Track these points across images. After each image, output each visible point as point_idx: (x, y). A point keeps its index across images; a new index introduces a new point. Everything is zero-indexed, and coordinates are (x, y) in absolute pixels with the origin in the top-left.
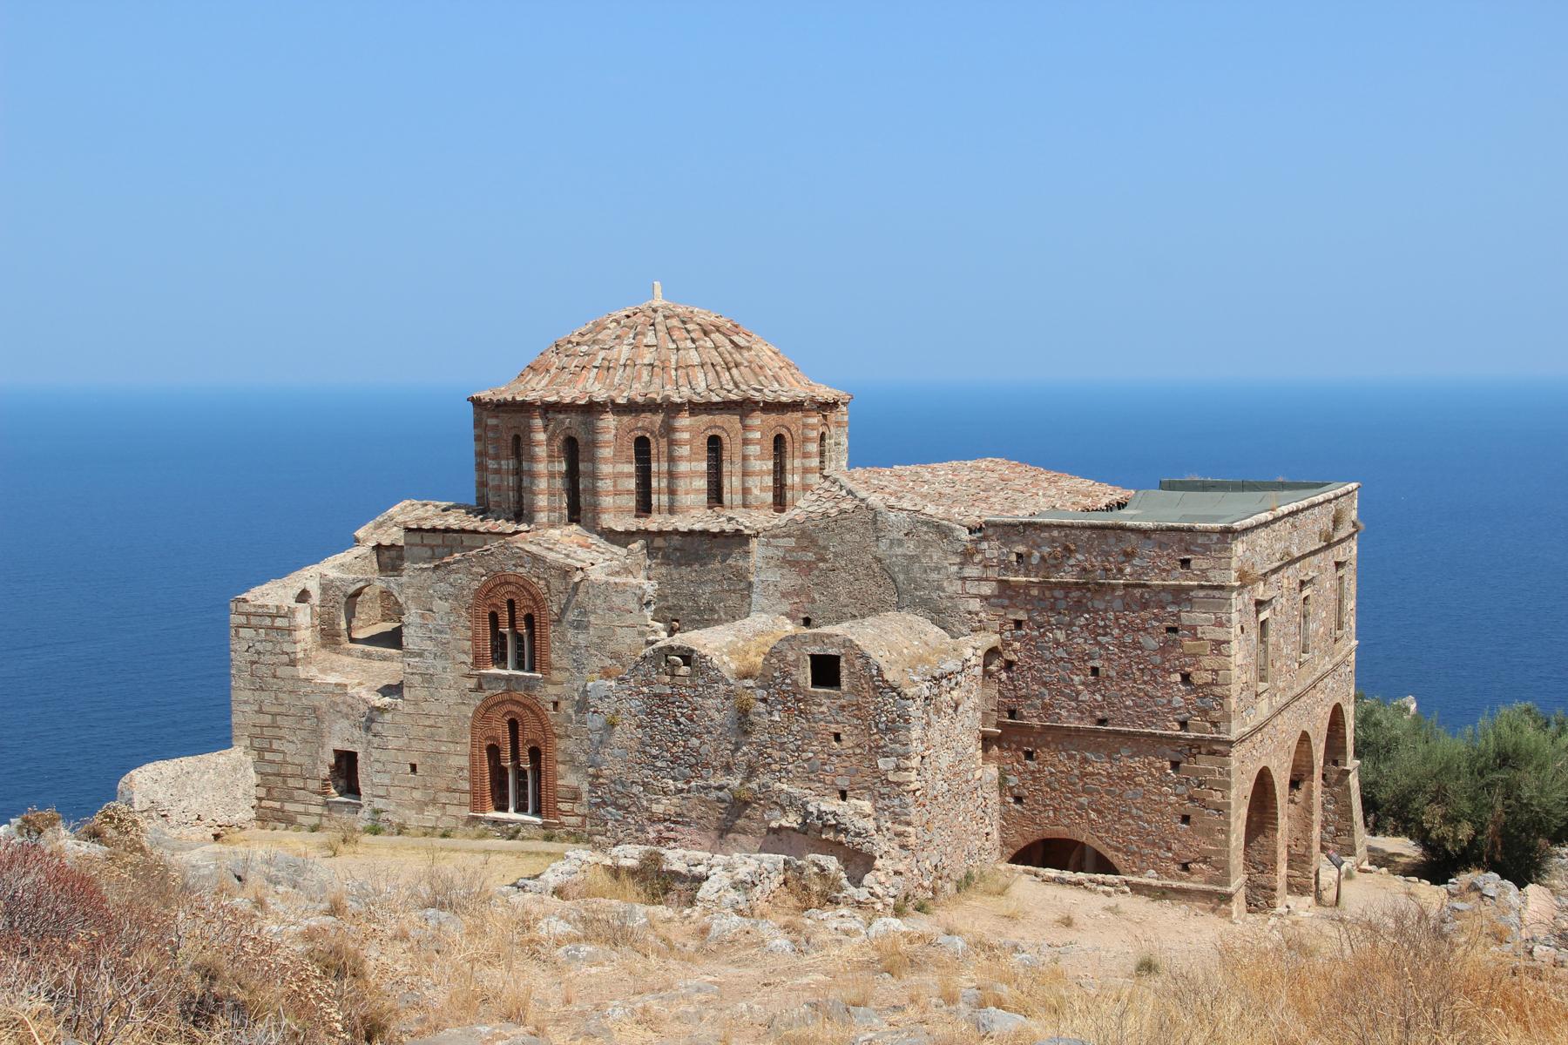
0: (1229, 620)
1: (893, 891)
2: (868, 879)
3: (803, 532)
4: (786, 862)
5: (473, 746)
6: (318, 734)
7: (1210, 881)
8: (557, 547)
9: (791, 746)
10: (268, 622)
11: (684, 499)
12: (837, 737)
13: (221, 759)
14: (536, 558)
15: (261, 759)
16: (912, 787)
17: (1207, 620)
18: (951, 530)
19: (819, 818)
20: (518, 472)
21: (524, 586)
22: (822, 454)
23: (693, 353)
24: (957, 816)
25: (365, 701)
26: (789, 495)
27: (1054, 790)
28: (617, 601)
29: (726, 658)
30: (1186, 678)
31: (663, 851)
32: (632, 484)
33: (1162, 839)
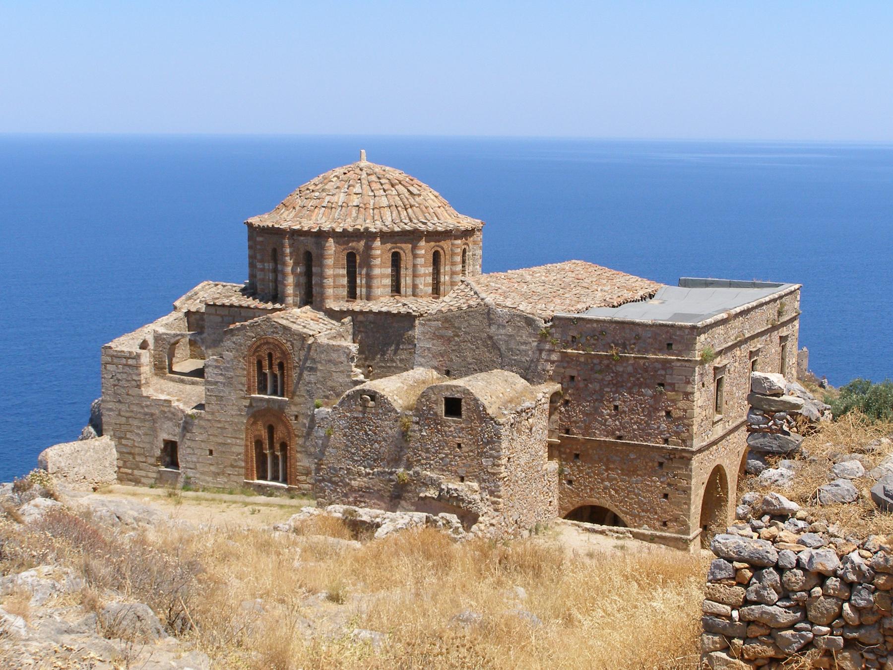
0: (694, 381)
1: (488, 535)
2: (474, 527)
3: (446, 319)
4: (427, 518)
5: (247, 440)
6: (154, 431)
7: (678, 532)
8: (298, 321)
9: (433, 450)
10: (124, 361)
11: (377, 292)
12: (459, 446)
13: (97, 443)
14: (285, 328)
15: (120, 443)
16: (502, 475)
17: (681, 380)
18: (534, 321)
19: (448, 492)
20: (275, 271)
21: (278, 346)
22: (464, 262)
23: (384, 198)
24: (531, 492)
25: (183, 411)
26: (442, 288)
27: (591, 477)
28: (334, 356)
29: (395, 397)
30: (668, 414)
31: (357, 509)
32: (345, 281)
33: (652, 507)
